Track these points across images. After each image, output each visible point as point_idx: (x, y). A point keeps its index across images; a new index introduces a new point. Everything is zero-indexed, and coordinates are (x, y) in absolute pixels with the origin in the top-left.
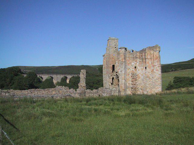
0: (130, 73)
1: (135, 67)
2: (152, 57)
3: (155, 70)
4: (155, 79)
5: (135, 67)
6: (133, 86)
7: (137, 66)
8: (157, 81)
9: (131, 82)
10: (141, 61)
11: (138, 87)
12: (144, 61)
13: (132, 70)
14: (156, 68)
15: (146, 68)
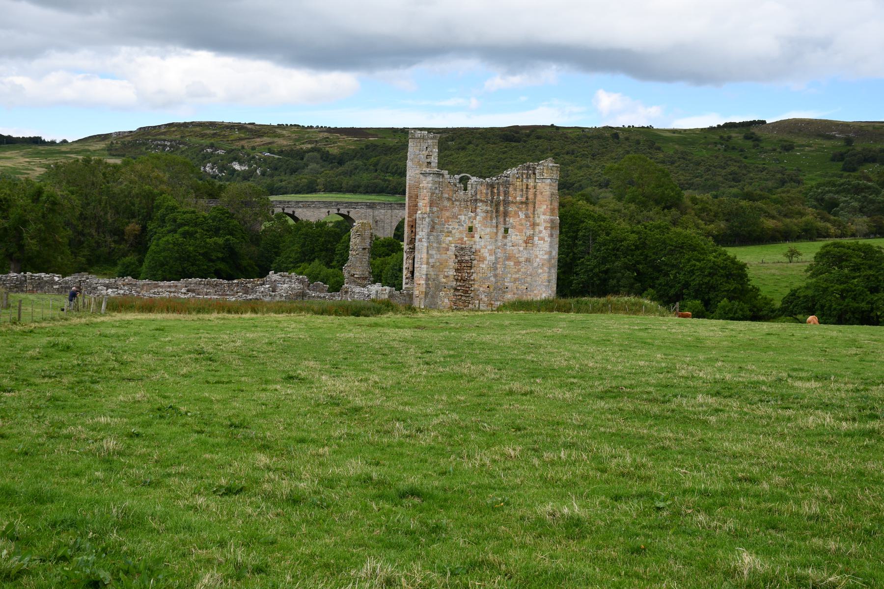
0: (453, 245)
1: (471, 229)
2: (531, 196)
3: (536, 238)
4: (535, 264)
5: (471, 229)
6: (458, 284)
7: (477, 224)
8: (540, 271)
9: (452, 273)
10: (489, 208)
11: (476, 286)
12: (501, 208)
13: (458, 235)
14: (540, 232)
15: (506, 231)
